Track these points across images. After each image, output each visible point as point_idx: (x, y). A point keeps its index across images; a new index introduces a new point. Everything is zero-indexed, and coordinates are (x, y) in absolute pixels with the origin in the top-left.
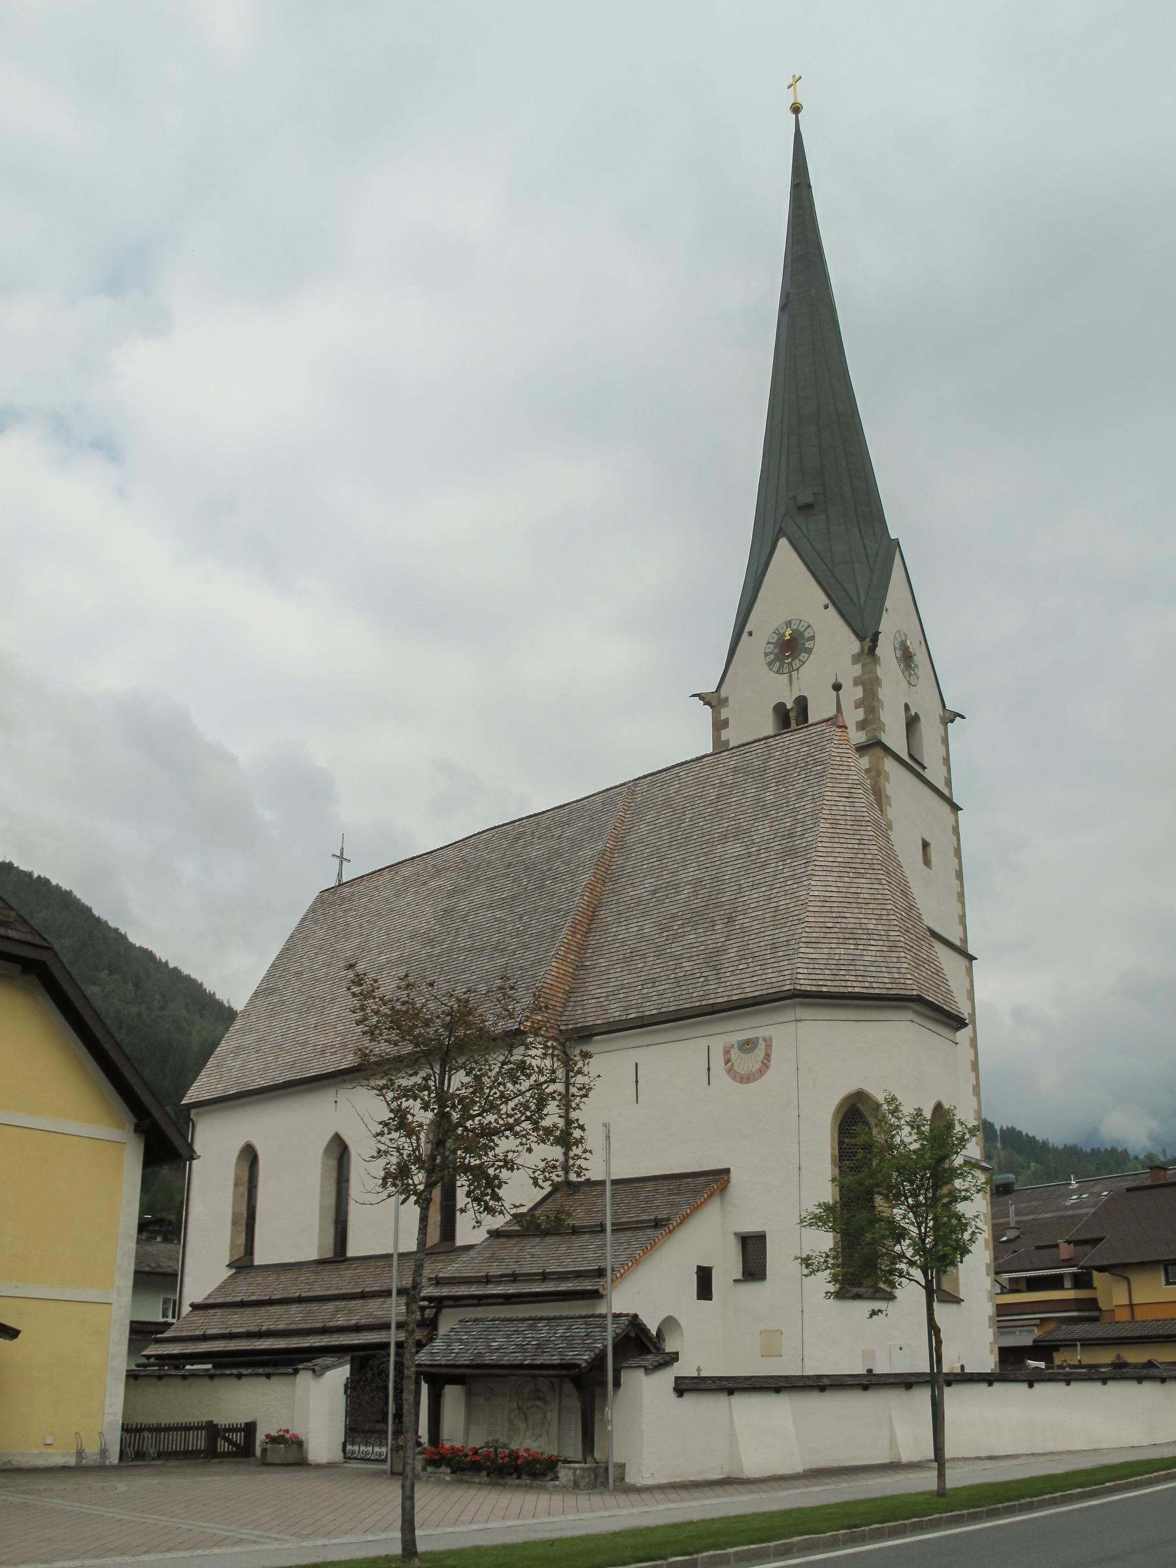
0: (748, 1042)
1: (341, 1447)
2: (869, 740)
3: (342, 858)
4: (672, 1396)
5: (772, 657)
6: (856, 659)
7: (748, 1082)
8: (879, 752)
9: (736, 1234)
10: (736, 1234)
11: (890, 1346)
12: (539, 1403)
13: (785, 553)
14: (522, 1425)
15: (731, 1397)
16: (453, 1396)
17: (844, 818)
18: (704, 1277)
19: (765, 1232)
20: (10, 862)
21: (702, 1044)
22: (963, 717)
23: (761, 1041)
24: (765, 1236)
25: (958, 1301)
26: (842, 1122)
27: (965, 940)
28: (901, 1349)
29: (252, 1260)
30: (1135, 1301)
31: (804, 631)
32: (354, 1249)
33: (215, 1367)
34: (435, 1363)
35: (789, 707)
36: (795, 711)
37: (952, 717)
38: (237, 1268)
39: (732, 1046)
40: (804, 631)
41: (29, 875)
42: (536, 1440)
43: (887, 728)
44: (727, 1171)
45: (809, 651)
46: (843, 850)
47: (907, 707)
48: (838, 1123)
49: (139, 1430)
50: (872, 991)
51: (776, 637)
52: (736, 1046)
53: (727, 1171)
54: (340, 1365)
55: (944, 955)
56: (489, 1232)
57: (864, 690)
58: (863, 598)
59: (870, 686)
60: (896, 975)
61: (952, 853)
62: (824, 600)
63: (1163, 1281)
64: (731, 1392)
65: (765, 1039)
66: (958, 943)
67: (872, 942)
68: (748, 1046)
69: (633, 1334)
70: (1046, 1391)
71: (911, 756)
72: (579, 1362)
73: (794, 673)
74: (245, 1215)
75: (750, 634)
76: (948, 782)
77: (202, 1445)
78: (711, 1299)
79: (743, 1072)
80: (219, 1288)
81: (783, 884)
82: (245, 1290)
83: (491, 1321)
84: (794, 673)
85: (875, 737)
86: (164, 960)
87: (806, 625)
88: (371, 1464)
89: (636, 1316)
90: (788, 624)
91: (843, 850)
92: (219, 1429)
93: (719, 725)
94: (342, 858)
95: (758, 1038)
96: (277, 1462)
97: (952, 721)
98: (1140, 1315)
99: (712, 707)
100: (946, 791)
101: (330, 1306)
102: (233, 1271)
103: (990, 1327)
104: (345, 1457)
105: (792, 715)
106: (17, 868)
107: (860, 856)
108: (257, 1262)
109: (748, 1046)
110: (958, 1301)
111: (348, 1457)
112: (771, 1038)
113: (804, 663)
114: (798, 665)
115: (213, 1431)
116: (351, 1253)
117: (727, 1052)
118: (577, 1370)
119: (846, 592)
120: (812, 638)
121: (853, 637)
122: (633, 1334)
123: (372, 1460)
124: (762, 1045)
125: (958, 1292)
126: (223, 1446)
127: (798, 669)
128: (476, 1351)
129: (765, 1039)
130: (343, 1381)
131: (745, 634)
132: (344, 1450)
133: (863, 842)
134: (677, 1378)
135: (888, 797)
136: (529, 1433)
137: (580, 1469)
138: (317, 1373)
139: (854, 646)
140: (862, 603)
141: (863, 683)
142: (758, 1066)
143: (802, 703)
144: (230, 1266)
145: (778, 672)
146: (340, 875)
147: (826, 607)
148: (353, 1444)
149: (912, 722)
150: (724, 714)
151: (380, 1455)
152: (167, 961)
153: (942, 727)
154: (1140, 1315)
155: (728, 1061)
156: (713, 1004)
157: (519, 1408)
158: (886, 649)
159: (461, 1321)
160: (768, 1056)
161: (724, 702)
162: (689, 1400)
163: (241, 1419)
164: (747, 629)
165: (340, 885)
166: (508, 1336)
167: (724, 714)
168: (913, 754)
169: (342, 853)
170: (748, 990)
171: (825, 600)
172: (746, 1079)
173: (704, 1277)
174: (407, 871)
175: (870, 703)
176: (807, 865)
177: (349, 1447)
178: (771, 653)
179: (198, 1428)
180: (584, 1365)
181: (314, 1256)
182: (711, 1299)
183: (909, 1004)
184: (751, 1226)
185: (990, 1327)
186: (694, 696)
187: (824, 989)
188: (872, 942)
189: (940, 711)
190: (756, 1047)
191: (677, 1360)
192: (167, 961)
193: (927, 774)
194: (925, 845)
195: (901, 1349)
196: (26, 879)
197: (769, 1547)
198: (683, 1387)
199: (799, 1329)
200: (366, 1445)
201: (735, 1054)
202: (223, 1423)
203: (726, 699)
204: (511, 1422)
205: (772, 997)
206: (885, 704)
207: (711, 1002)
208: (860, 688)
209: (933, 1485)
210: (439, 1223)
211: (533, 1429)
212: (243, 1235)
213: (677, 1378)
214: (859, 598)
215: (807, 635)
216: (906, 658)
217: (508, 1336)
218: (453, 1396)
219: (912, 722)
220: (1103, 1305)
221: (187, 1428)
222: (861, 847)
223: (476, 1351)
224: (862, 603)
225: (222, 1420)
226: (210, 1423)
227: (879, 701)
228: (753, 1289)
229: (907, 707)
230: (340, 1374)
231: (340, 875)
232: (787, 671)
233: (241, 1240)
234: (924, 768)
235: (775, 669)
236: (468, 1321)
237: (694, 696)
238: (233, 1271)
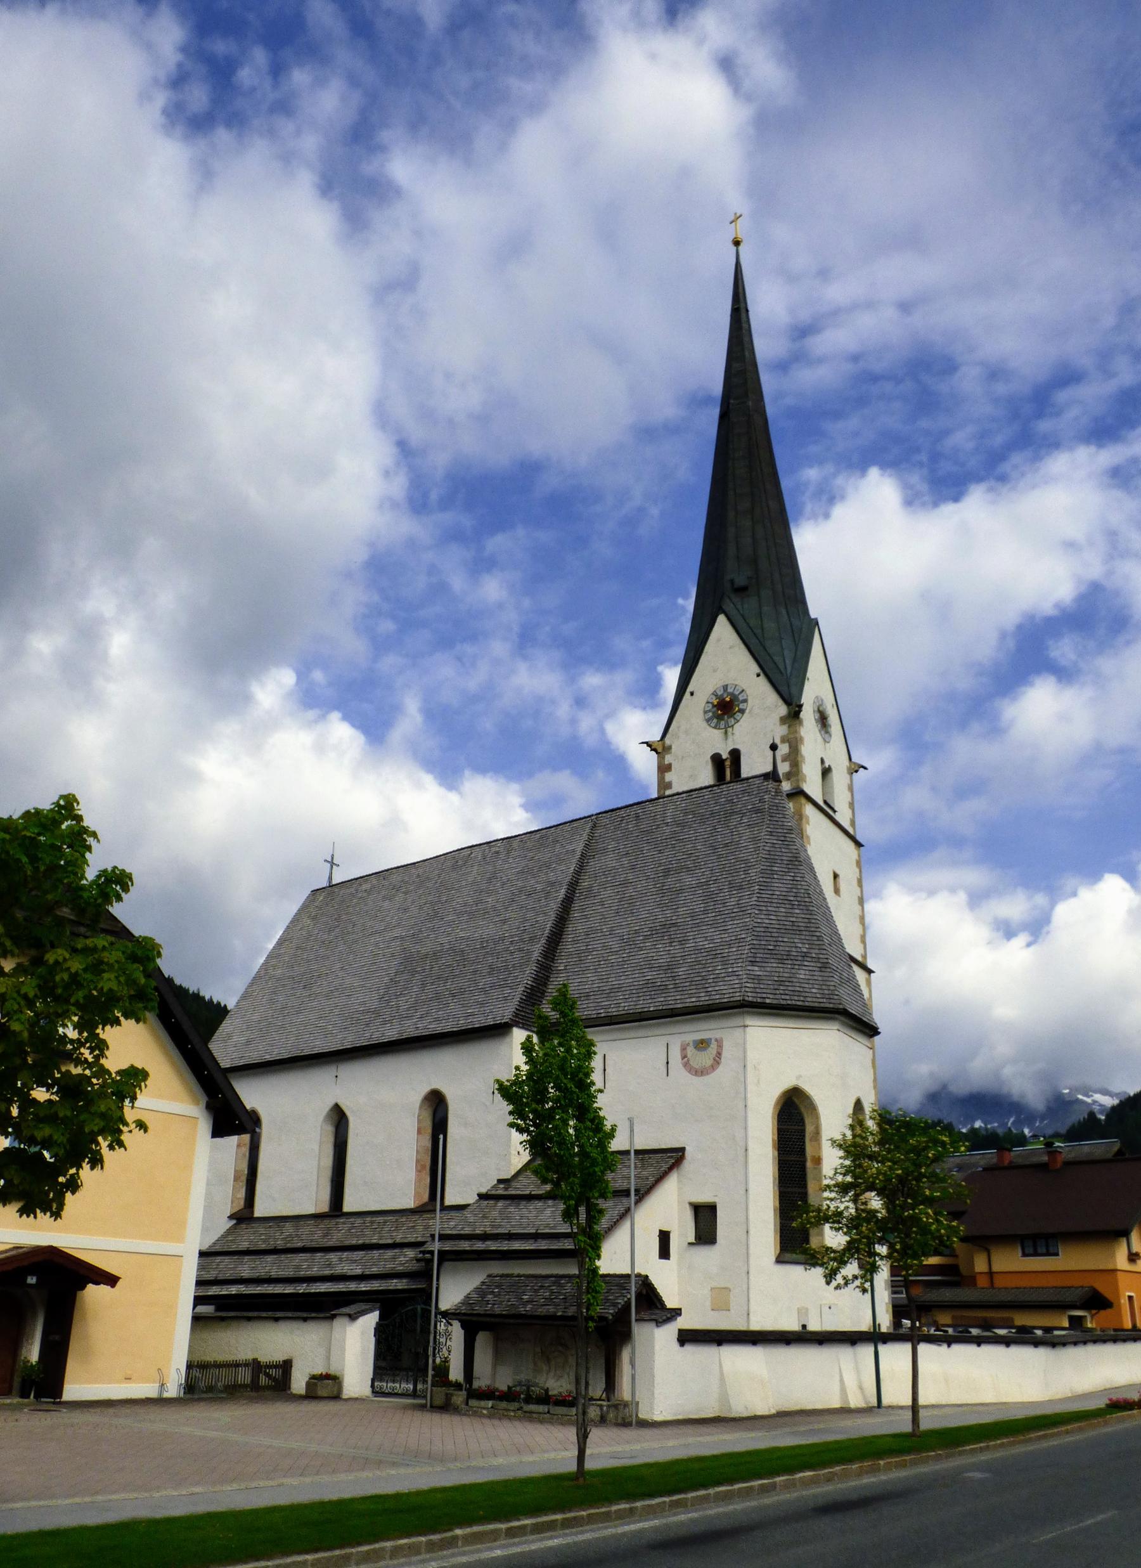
0: (702, 1042)
1: (370, 1382)
2: (793, 789)
3: (332, 864)
4: (676, 1345)
5: (711, 714)
6: (783, 720)
7: (702, 1075)
8: (803, 800)
9: (691, 1204)
10: (691, 1204)
11: (821, 1305)
12: (560, 1348)
13: (722, 631)
14: (545, 1368)
15: (720, 1347)
16: (482, 1340)
17: (781, 858)
18: (664, 1238)
19: (715, 1202)
21: (663, 1040)
22: (865, 768)
23: (713, 1041)
24: (715, 1206)
26: (780, 1112)
27: (865, 957)
28: (830, 1308)
29: (252, 1212)
30: (995, 1268)
31: (739, 694)
32: (350, 1204)
33: (217, 1310)
34: (475, 1312)
35: (724, 757)
36: (729, 760)
37: (856, 769)
38: (237, 1219)
39: (688, 1044)
40: (739, 694)
42: (558, 1380)
43: (808, 779)
45: (742, 711)
46: (780, 885)
47: (822, 761)
48: (777, 1113)
49: (204, 1366)
50: (807, 1004)
52: (691, 1044)
54: (371, 1311)
55: (856, 969)
56: (478, 1195)
57: (790, 747)
58: (789, 671)
59: (795, 744)
60: (826, 992)
61: (855, 883)
62: (757, 670)
63: (1020, 1254)
64: (720, 1343)
65: (716, 1040)
66: (859, 958)
67: (806, 963)
68: (702, 1045)
69: (644, 1292)
70: (987, 1350)
71: (825, 802)
72: (607, 1315)
73: (730, 730)
74: (246, 1172)
75: (692, 694)
76: (853, 823)
77: (248, 1380)
78: (669, 1259)
79: (697, 1067)
80: (223, 1236)
81: (730, 911)
82: (247, 1239)
83: (516, 1277)
84: (730, 730)
85: (798, 787)
87: (740, 690)
88: (392, 1398)
89: (647, 1276)
90: (725, 687)
91: (780, 885)
92: (261, 1366)
93: (664, 769)
94: (332, 864)
95: (711, 1039)
96: (326, 1395)
97: (856, 771)
98: (999, 1282)
99: (657, 753)
100: (851, 830)
101: (333, 1257)
102: (234, 1222)
104: (373, 1392)
105: (728, 763)
107: (794, 890)
108: (257, 1214)
109: (702, 1045)
111: (376, 1392)
112: (722, 1039)
113: (738, 721)
114: (733, 723)
115: (256, 1366)
116: (346, 1208)
117: (684, 1049)
118: (605, 1323)
119: (775, 663)
120: (745, 701)
121: (780, 702)
122: (644, 1292)
123: (399, 1394)
124: (714, 1045)
126: (263, 1380)
127: (733, 726)
128: (510, 1303)
129: (716, 1040)
130: (373, 1325)
131: (687, 694)
132: (372, 1386)
133: (796, 879)
134: (680, 1331)
135: (808, 837)
136: (552, 1374)
138: (353, 1318)
139: (783, 710)
140: (789, 675)
141: (788, 741)
143: (735, 755)
144: (231, 1217)
145: (715, 728)
146: (330, 878)
147: (758, 675)
148: (381, 1381)
149: (826, 772)
150: (668, 759)
151: (381, 1388)
153: (848, 776)
154: (999, 1282)
155: (684, 1057)
156: (672, 1009)
157: (542, 1352)
158: (808, 715)
159: (489, 1276)
160: (719, 1054)
161: (667, 749)
162: (689, 1348)
163: (279, 1357)
164: (690, 689)
165: (330, 886)
166: (536, 1291)
167: (668, 759)
168: (828, 801)
169: (332, 858)
170: (703, 999)
171: (757, 670)
172: (700, 1072)
173: (664, 1238)
174: (395, 878)
175: (794, 758)
176: (751, 896)
177: (376, 1384)
178: (709, 711)
179: (246, 1364)
180: (611, 1317)
181: (311, 1210)
182: (669, 1259)
183: (837, 1016)
184: (703, 1198)
186: (643, 743)
187: (768, 1001)
188: (806, 963)
189: (847, 763)
190: (709, 1046)
191: (680, 1315)
193: (837, 817)
194: (836, 876)
195: (830, 1308)
197: (819, 1475)
198: (687, 1337)
199: (745, 1286)
200: (394, 1382)
201: (690, 1051)
202: (265, 1361)
203: (670, 748)
204: (535, 1364)
205: (727, 1005)
206: (806, 759)
207: (671, 1007)
208: (787, 745)
209: (596, 1435)
210: (428, 1185)
211: (555, 1370)
212: (243, 1191)
213: (680, 1331)
214: (786, 668)
215: (741, 698)
216: (823, 719)
217: (536, 1291)
218: (482, 1340)
219: (826, 772)
220: (964, 1270)
221: (236, 1365)
222: (795, 882)
223: (510, 1303)
225: (264, 1358)
226: (255, 1361)
227: (802, 756)
228: (704, 1254)
229: (822, 761)
230: (371, 1320)
231: (330, 878)
232: (723, 726)
233: (242, 1194)
234: (835, 811)
235: (713, 725)
236: (496, 1277)
237: (643, 743)
238: (234, 1222)
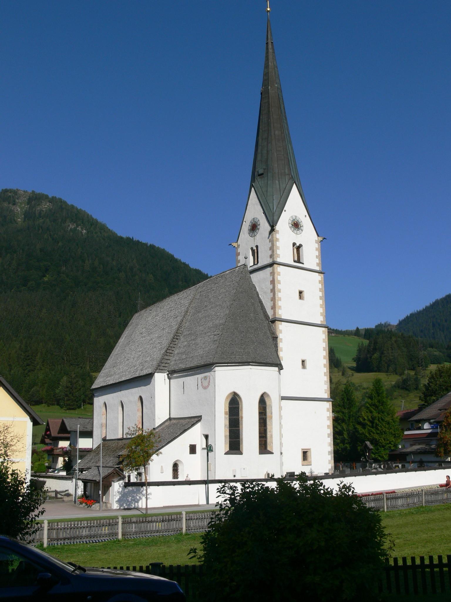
20: (138, 240)
25: (272, 453)
41: (146, 245)
44: (201, 416)
51: (251, 223)
53: (201, 416)
73: (255, 237)
86: (206, 273)
103: (329, 455)
106: (141, 242)
109: (205, 378)
110: (272, 453)
125: (272, 450)
137: (425, 497)
140: (274, 211)
142: (207, 384)
152: (207, 274)
155: (202, 382)
164: (244, 220)
179: (53, 492)
185: (329, 455)
192: (207, 274)
196: (145, 247)
224: (274, 211)
